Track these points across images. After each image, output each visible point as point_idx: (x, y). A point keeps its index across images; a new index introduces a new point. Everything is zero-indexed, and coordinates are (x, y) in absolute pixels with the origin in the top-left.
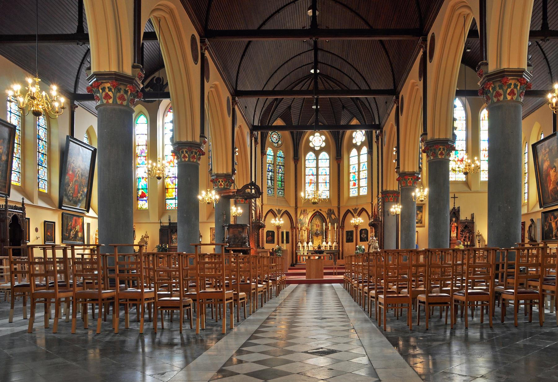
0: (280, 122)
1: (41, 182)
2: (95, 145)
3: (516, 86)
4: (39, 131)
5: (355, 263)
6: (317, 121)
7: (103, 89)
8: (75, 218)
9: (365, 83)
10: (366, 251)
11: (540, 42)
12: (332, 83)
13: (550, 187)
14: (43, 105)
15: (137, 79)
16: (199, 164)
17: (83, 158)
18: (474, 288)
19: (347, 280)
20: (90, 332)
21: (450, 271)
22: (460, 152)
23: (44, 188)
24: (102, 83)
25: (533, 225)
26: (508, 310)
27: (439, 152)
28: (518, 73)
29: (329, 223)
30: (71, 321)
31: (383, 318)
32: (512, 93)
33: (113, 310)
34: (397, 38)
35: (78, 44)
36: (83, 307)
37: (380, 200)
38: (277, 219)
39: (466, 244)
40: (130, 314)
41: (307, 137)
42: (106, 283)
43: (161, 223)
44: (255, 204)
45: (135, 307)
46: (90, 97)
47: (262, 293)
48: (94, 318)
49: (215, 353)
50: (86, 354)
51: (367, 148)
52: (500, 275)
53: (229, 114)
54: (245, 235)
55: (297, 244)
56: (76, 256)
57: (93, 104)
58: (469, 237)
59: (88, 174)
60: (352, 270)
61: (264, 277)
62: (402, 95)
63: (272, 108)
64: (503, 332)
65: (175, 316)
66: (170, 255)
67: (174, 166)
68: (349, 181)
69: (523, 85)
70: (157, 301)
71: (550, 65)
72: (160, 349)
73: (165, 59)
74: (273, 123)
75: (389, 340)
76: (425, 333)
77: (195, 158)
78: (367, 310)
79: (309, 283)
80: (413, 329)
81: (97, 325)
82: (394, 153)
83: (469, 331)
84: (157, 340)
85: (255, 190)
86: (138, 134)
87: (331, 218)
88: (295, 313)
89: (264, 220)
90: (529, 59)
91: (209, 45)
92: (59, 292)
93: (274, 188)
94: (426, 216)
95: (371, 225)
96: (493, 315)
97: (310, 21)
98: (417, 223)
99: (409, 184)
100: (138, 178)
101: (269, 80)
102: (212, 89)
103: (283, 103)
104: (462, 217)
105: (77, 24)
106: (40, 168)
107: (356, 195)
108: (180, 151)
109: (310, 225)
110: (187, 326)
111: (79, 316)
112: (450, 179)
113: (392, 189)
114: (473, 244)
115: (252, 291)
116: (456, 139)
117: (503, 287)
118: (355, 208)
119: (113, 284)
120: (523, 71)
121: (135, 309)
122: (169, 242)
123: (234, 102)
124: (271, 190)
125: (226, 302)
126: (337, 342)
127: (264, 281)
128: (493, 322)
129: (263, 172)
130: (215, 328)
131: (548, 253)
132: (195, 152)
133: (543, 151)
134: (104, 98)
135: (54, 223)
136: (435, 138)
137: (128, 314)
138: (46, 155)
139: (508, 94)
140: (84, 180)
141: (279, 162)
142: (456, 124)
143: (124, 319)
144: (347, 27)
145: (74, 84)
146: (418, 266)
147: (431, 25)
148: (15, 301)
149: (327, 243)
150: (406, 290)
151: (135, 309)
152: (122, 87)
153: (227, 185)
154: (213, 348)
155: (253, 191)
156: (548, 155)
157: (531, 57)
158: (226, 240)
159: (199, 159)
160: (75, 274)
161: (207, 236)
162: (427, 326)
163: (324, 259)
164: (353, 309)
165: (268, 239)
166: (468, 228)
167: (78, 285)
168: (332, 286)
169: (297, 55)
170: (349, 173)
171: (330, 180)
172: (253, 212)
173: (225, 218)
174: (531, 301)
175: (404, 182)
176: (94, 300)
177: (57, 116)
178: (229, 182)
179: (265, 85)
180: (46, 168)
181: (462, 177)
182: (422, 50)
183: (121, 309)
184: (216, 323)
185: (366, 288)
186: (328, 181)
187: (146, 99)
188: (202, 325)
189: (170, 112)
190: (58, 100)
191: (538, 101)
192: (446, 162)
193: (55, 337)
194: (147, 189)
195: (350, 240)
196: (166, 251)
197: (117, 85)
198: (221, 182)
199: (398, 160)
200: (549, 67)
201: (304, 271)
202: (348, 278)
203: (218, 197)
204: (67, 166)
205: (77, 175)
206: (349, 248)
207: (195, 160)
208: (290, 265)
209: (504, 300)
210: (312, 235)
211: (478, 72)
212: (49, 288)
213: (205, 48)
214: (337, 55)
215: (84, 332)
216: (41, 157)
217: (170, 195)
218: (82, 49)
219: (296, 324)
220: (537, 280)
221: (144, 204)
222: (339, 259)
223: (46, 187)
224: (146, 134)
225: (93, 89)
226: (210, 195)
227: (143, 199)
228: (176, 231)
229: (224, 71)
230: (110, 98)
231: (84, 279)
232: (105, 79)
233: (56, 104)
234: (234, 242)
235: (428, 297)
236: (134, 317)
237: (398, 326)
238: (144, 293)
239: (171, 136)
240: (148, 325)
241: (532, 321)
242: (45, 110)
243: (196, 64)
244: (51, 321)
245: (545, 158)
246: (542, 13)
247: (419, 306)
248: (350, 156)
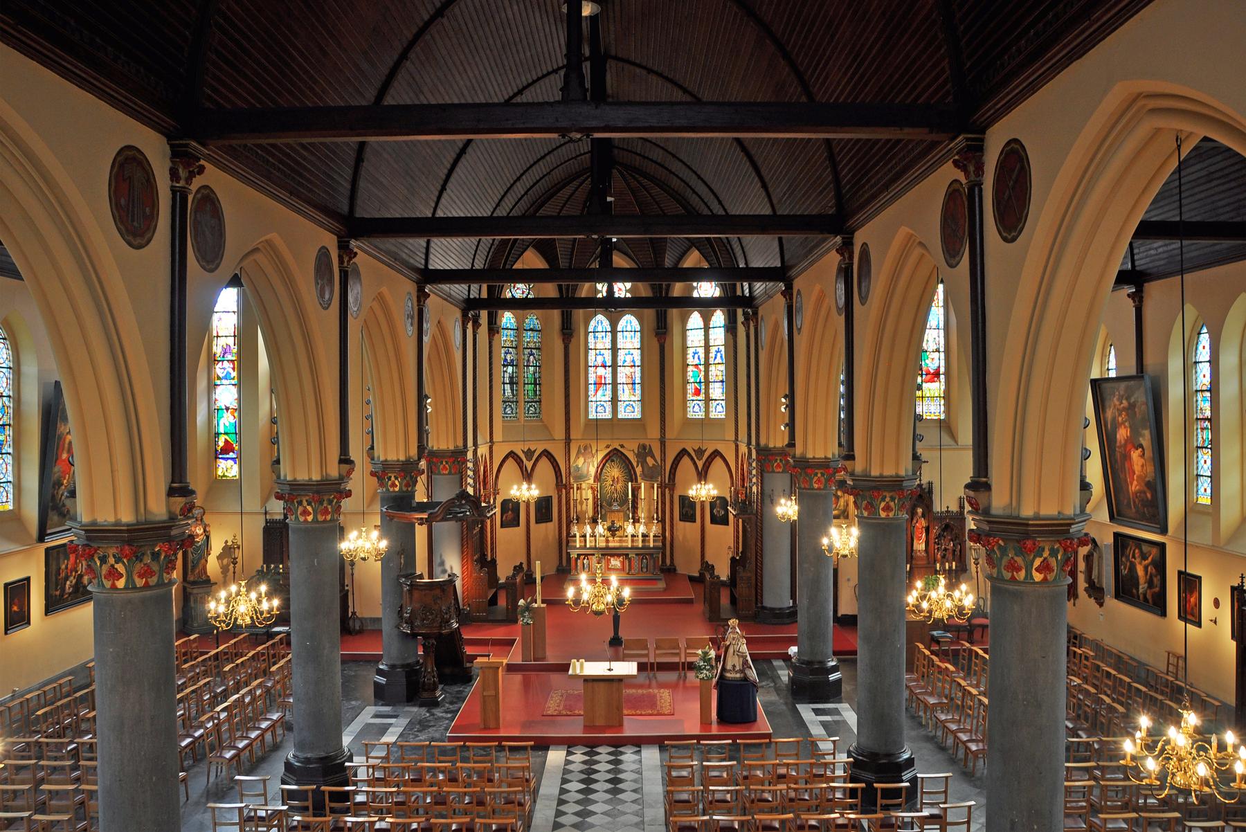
58: (954, 551)
68: (685, 382)
77: (329, 513)
82: (783, 410)
100: (218, 410)
107: (701, 415)
124: (510, 406)
129: (494, 366)
139: (1037, 570)
141: (528, 342)
166: (952, 530)
171: (642, 378)
186: (638, 380)
194: (236, 434)
198: (393, 479)
210: (601, 508)
221: (229, 466)
223: (11, 496)
224: (234, 312)
227: (227, 456)
248: (688, 328)
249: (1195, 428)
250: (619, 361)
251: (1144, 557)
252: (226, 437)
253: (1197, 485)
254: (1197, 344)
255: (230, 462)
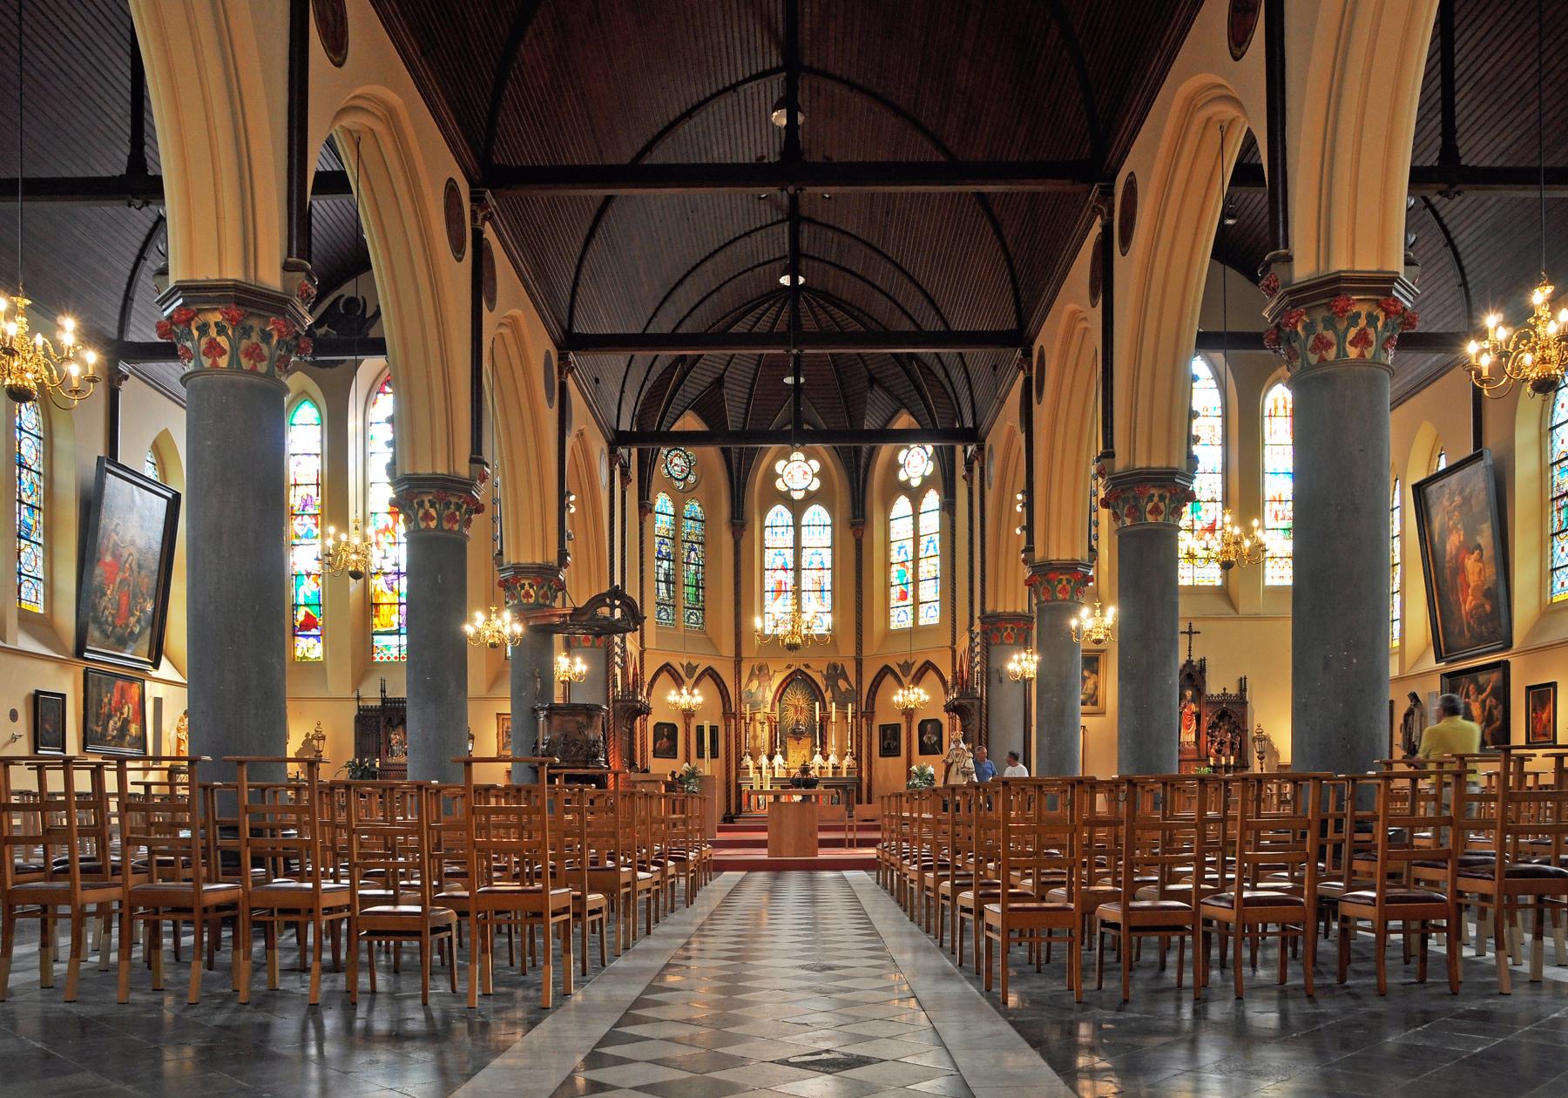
0: (693, 421)
1: (26, 584)
2: (180, 484)
3: (1372, 320)
4: (22, 445)
5: (911, 814)
6: (798, 419)
7: (203, 329)
8: (120, 683)
9: (933, 313)
10: (939, 783)
11: (1435, 199)
12: (839, 315)
13: (1465, 603)
14: (36, 372)
15: (297, 301)
16: (466, 536)
17: (142, 517)
18: (1259, 885)
19: (887, 861)
20: (169, 1000)
21: (1187, 842)
22: (1205, 506)
23: (34, 599)
24: (200, 311)
25: (1416, 711)
26: (1356, 948)
27: (1150, 506)
28: (1380, 285)
29: (831, 703)
30: (116, 967)
31: (997, 967)
32: (1362, 340)
33: (235, 938)
34: (1027, 188)
35: (130, 206)
36: (148, 929)
37: (978, 640)
38: (684, 691)
39: (1223, 762)
40: (280, 949)
41: (892, 456)
42: (213, 862)
43: (358, 698)
44: (624, 649)
45: (294, 930)
46: (166, 351)
47: (648, 895)
48: (177, 959)
49: (527, 1062)
50: (159, 1061)
51: (939, 494)
52: (1329, 849)
53: (550, 399)
54: (595, 734)
55: (739, 760)
56: (131, 789)
57: (171, 371)
58: (1232, 744)
59: (157, 563)
60: (904, 834)
61: (650, 850)
62: (1042, 347)
63: (669, 384)
64: (1346, 1011)
65: (405, 958)
66: (392, 789)
67: (395, 543)
68: (888, 585)
69: (1393, 317)
70: (358, 913)
71: (1465, 263)
72: (370, 1049)
73: (374, 248)
74: (673, 424)
75: (1019, 1032)
76: (1119, 1010)
77: (457, 521)
78: (948, 945)
79: (777, 868)
80: (1084, 1000)
81: (188, 981)
82: (1019, 509)
83: (1247, 1005)
84: (359, 1024)
85: (622, 611)
86: (294, 455)
87: (836, 689)
88: (741, 954)
89: (648, 694)
90: (1409, 247)
91: (494, 207)
92: (84, 888)
93: (674, 606)
94: (1109, 685)
95: (951, 708)
96: (1314, 962)
97: (777, 141)
98: (1084, 703)
99: (1060, 596)
100: (296, 576)
101: (661, 304)
102: (504, 330)
103: (698, 370)
104: (1213, 688)
105: (128, 151)
106: (22, 547)
107: (909, 623)
108: (415, 501)
109: (777, 708)
110: (442, 986)
111: (138, 953)
112: (1181, 582)
113: (1010, 609)
114: (1243, 764)
115: (623, 891)
116: (1197, 469)
117: (1342, 884)
118: (906, 662)
119: (231, 865)
120: (1393, 278)
121: (292, 936)
122: (383, 752)
123: (565, 366)
124: (666, 610)
125: (552, 920)
126: (869, 1033)
127: (654, 863)
128: (1316, 981)
130: (519, 993)
131: (1530, 788)
132: (457, 503)
133: (1446, 503)
134: (204, 354)
135: (63, 696)
136: (1137, 466)
137: (277, 951)
138: (39, 509)
140: (146, 580)
141: (688, 534)
142: (1198, 426)
143: (265, 964)
144: (881, 156)
145: (117, 317)
146: (1095, 823)
147: (1126, 151)
148: (1429, 941)
149: (826, 758)
150: (1062, 891)
151: (292, 936)
152: (255, 323)
153: (545, 596)
154: (518, 1046)
155: (618, 613)
156: (1460, 513)
157: (1414, 238)
158: (541, 747)
159: (468, 523)
160: (128, 838)
161: (487, 738)
162: (1126, 991)
163: (817, 800)
164: (909, 941)
165: (658, 745)
166: (1231, 717)
167: (133, 868)
168: (843, 877)
169: (740, 237)
170: (888, 564)
171: (833, 583)
172: (618, 671)
173: (539, 686)
174: (1424, 924)
175: (1045, 588)
176: (182, 910)
177: (76, 402)
178: (550, 588)
179: (650, 320)
180: (39, 544)
181: (1212, 575)
182: (1099, 221)
183: (257, 938)
184: (523, 978)
185: (947, 884)
186: (828, 586)
187: (319, 358)
188: (484, 984)
189: (385, 393)
190: (77, 358)
191: (1429, 363)
192: (1167, 535)
193: (71, 1012)
194: (320, 605)
195: (890, 750)
196: (373, 775)
197: (241, 318)
198: (527, 587)
199: (1029, 529)
200: (1462, 269)
201: (763, 836)
202: (891, 855)
203: (518, 629)
204: (99, 541)
205: (127, 565)
206: (889, 772)
207: (456, 527)
208: (721, 817)
209: (1345, 919)
210: (782, 738)
211: (1263, 282)
212: (54, 876)
213: (484, 216)
214: (854, 237)
215: (153, 998)
216: (26, 514)
217: (383, 622)
218: (142, 218)
219: (747, 984)
220: (1440, 864)
221: (311, 646)
222: (859, 801)
223: (41, 597)
224: (317, 455)
225: (174, 327)
226: (497, 623)
227: (309, 633)
228: (403, 721)
229: (538, 280)
230: (223, 352)
231: (151, 853)
232: (208, 301)
233: (74, 370)
234: (566, 751)
235: (1127, 911)
236: (291, 959)
237: (1042, 991)
238: (320, 892)
239: (389, 460)
240: (332, 981)
241: (1428, 980)
242: (41, 386)
243: (459, 260)
244: (60, 968)
245: (1451, 523)
246: (1439, 117)
247: (1102, 934)
249: (1550, 511)
250: (803, 563)
251: (1480, 690)
252: (307, 609)
253: (1552, 582)
254: (1554, 404)
255: (312, 641)
